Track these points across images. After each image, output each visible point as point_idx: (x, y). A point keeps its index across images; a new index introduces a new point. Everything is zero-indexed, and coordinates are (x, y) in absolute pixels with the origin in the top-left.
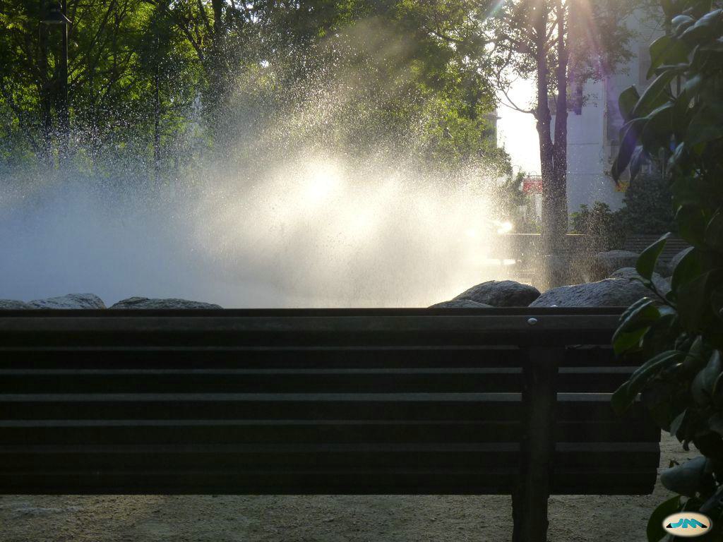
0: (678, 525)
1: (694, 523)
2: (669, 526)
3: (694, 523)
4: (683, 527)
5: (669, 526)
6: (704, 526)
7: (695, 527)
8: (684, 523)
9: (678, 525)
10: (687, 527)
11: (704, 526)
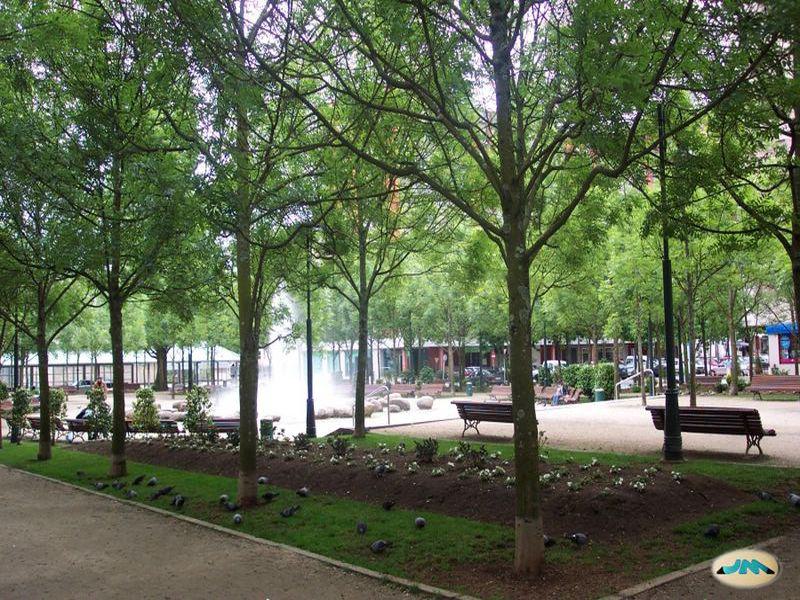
0: (732, 569)
1: (756, 566)
2: (721, 571)
3: (756, 566)
5: (721, 571)
6: (769, 572)
8: (742, 567)
9: (732, 569)
11: (769, 572)
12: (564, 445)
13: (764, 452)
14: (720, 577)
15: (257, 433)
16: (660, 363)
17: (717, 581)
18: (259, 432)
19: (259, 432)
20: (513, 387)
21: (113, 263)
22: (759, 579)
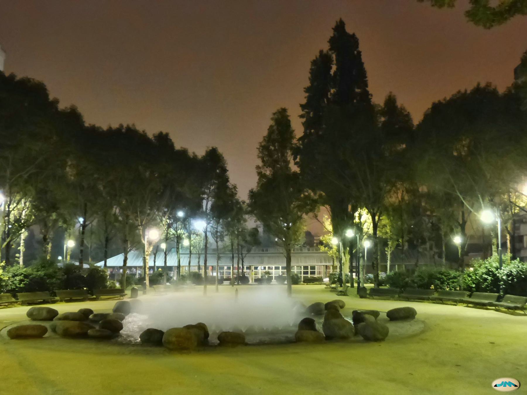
0: (501, 385)
1: (510, 384)
2: (496, 386)
3: (510, 384)
4: (504, 386)
5: (496, 386)
6: (516, 386)
7: (511, 386)
8: (504, 384)
9: (501, 385)
10: (506, 386)
11: (516, 386)
12: (461, 305)
13: (217, 261)
14: (495, 388)
15: (390, 258)
16: (170, 222)
17: (494, 390)
18: (389, 259)
19: (389, 259)
20: (370, 214)
21: (54, 241)
22: (508, 389)
